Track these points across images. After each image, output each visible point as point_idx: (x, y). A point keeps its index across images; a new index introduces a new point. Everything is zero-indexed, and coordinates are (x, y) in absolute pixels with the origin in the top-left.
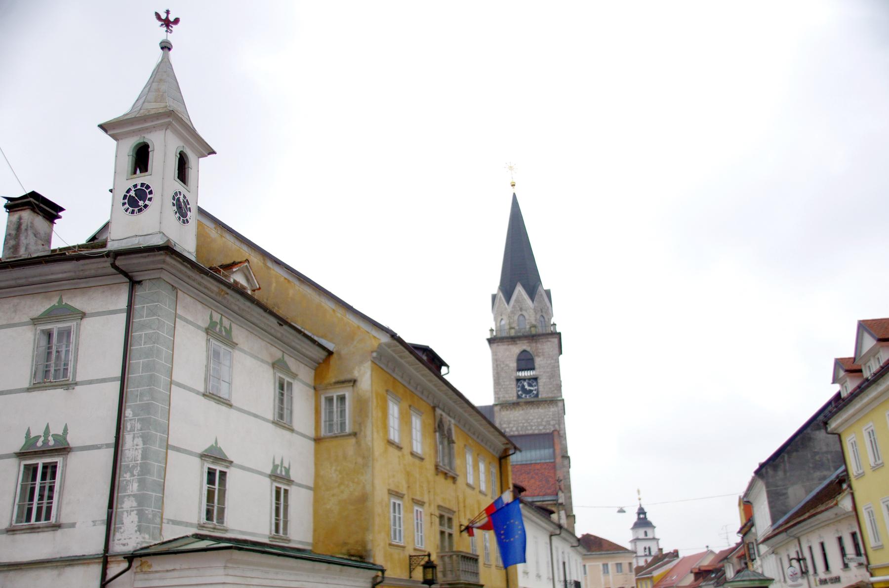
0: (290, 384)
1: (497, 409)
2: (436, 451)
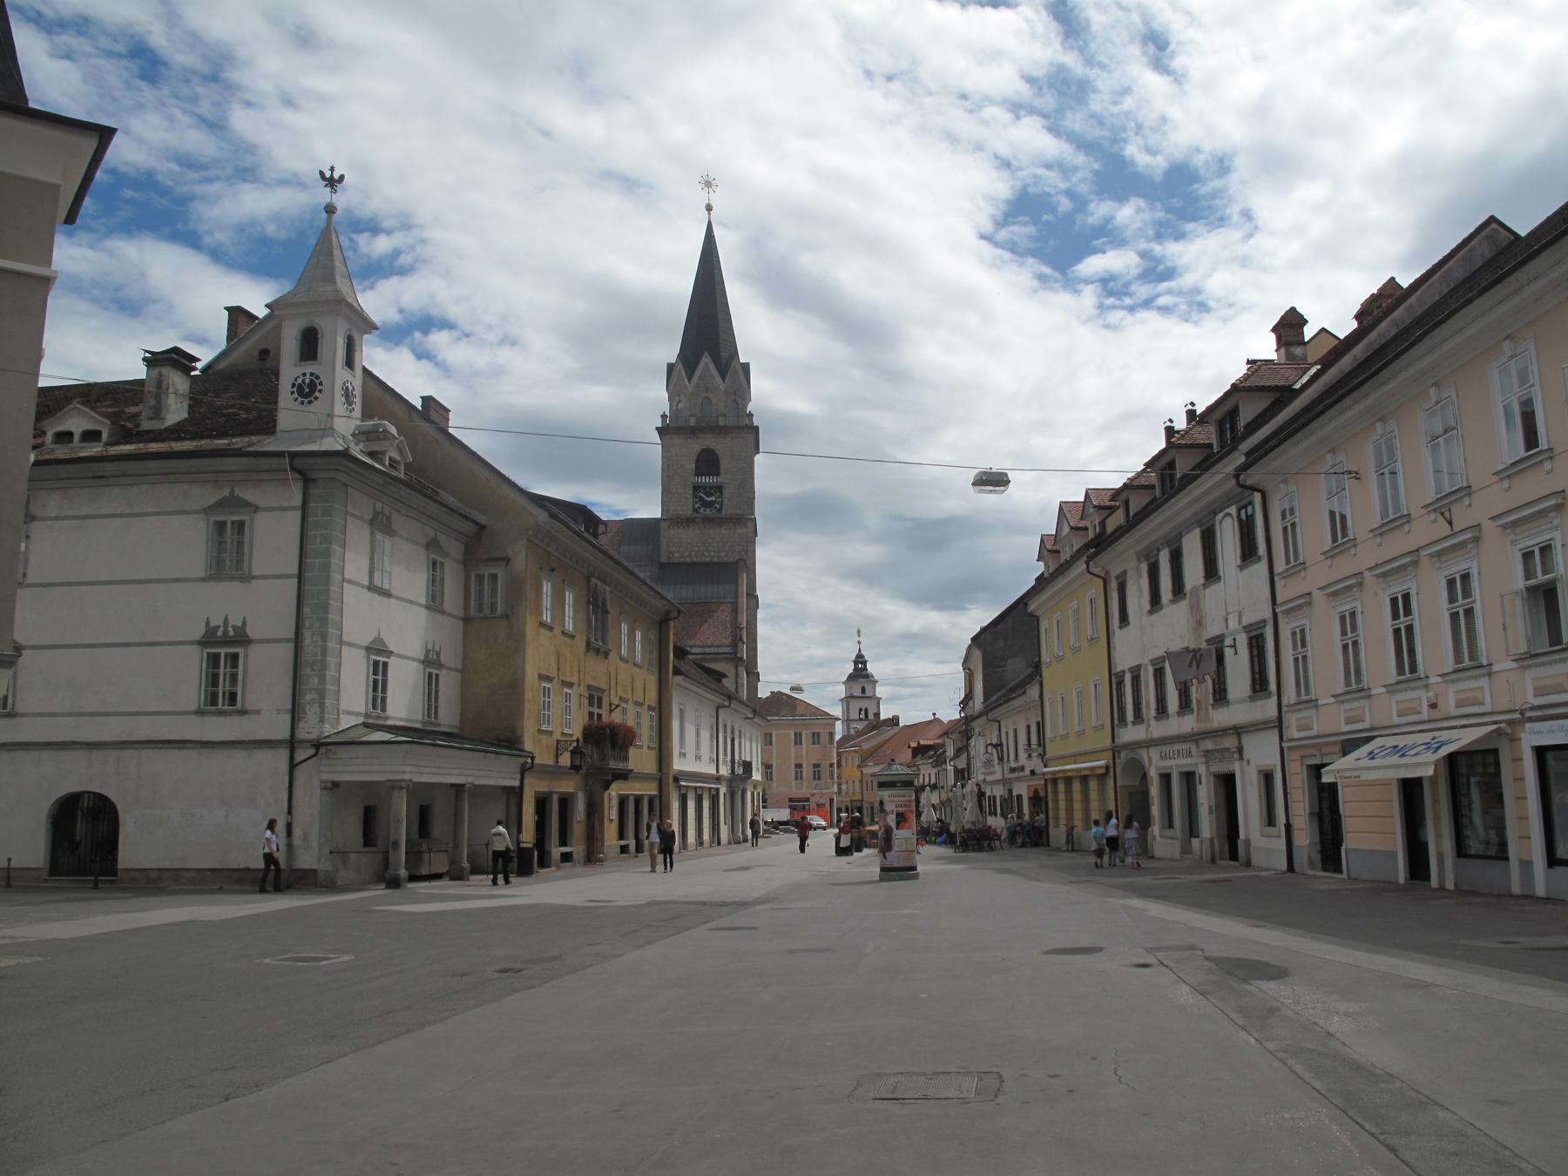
0: (442, 564)
1: (664, 525)
2: (589, 626)
